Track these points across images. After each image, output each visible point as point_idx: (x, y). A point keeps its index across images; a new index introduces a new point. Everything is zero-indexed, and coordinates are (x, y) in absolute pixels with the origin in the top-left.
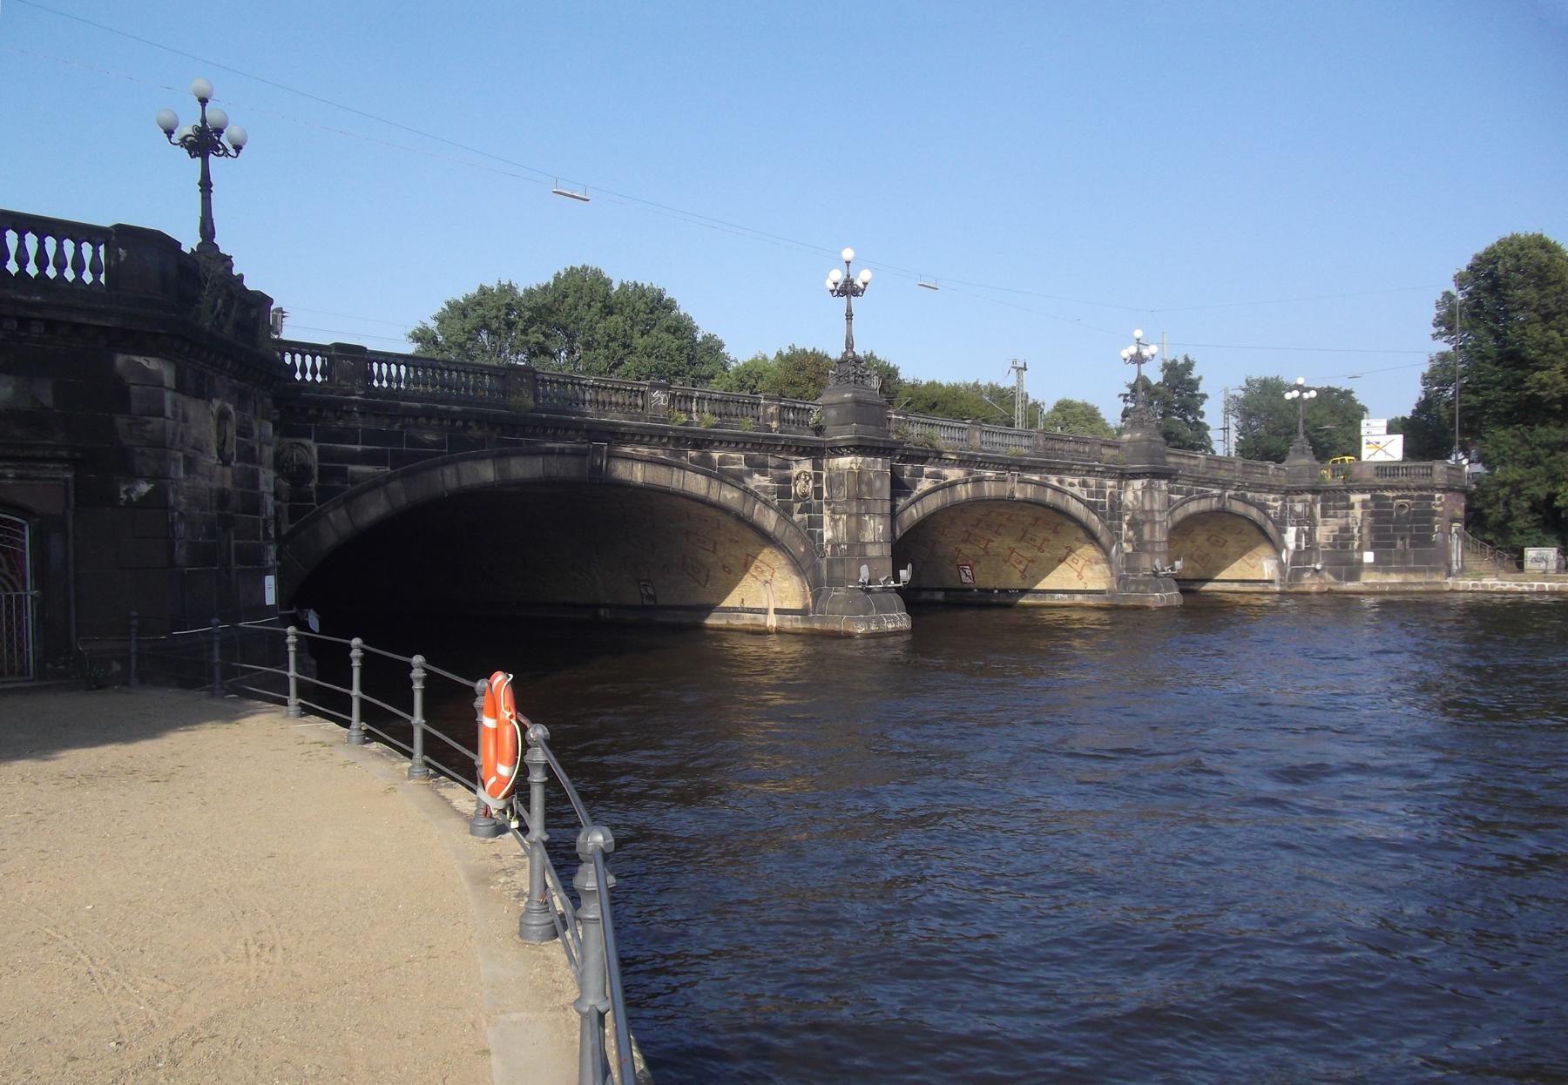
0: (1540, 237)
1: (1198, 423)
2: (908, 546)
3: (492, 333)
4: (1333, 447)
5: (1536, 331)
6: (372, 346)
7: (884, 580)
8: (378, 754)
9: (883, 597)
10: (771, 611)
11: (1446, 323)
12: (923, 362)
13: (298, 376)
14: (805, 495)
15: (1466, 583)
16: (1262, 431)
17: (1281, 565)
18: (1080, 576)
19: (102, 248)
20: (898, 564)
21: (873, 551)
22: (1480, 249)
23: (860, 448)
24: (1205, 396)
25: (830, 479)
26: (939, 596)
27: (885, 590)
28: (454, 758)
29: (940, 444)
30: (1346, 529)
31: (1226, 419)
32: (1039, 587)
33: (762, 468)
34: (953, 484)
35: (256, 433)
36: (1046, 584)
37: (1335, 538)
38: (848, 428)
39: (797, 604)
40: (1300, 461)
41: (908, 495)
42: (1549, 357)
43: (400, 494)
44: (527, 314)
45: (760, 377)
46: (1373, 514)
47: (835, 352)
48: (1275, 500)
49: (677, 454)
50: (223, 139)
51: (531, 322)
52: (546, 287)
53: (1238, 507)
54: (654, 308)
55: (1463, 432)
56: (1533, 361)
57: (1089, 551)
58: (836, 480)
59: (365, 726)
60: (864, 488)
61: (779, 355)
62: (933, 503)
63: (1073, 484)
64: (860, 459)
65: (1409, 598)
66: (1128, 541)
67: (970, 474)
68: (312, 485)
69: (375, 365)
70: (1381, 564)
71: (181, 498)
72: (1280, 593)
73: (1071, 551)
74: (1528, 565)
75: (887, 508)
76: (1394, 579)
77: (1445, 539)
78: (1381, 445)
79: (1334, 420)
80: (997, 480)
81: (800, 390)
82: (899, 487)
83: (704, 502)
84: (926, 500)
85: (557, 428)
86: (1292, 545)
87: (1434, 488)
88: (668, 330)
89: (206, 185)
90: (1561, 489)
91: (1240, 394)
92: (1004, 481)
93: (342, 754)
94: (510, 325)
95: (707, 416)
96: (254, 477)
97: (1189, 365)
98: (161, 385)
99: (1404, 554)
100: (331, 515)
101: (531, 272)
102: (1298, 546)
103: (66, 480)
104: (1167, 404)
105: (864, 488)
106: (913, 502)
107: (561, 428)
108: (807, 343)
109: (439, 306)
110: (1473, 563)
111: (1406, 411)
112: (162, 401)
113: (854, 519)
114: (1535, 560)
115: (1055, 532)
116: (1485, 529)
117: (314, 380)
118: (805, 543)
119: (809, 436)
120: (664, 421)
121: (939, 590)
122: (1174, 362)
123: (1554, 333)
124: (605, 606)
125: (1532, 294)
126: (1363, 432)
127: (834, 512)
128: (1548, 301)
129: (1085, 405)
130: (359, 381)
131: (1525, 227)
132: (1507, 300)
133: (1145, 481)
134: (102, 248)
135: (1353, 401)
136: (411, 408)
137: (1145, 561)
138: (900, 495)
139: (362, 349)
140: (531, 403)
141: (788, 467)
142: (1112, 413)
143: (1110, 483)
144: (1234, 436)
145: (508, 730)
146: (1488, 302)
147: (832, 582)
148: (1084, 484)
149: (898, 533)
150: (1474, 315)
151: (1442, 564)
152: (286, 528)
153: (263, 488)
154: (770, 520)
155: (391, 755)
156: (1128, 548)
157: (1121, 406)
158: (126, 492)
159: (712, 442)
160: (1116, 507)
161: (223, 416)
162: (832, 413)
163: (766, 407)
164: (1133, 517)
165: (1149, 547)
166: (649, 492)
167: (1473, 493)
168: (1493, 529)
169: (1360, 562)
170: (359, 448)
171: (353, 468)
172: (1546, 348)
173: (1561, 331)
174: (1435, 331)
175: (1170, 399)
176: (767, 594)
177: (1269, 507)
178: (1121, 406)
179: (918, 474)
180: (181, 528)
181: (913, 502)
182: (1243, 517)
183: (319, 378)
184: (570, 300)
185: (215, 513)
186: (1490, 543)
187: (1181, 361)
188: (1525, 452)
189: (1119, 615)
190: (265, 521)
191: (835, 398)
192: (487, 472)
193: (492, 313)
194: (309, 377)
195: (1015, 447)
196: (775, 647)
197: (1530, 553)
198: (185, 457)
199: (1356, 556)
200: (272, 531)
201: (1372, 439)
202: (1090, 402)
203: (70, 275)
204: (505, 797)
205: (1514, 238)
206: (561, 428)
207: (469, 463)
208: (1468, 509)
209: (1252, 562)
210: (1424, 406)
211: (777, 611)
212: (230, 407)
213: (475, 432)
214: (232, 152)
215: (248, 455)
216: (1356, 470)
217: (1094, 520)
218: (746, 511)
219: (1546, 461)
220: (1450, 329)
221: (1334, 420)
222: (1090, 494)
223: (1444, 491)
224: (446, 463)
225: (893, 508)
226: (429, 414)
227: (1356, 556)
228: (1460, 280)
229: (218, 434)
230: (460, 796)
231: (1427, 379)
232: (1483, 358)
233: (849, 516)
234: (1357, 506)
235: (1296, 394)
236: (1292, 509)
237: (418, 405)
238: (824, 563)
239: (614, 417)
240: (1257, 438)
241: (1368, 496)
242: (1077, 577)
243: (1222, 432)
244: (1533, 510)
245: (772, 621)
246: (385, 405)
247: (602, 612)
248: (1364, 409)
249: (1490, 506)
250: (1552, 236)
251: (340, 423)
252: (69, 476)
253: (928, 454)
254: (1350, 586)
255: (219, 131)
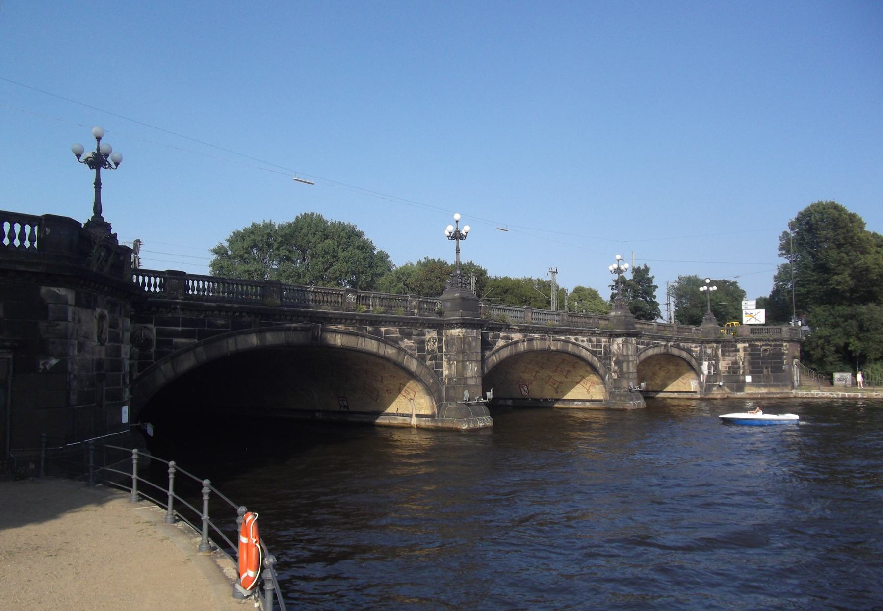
0: (834, 203)
1: (652, 301)
2: (491, 378)
3: (259, 249)
4: (727, 314)
5: (833, 253)
6: (189, 271)
7: (478, 398)
8: (182, 531)
9: (477, 407)
10: (414, 416)
11: (786, 247)
12: (500, 266)
13: (146, 289)
14: (433, 350)
15: (803, 393)
16: (688, 305)
17: (700, 383)
18: (588, 392)
19: (36, 228)
20: (485, 390)
21: (472, 382)
22: (802, 209)
23: (463, 324)
24: (656, 287)
25: (447, 341)
26: (510, 402)
27: (478, 404)
28: (225, 540)
29: (509, 320)
30: (735, 363)
31: (668, 299)
32: (565, 397)
33: (409, 336)
34: (516, 342)
35: (121, 325)
36: (569, 396)
37: (730, 368)
38: (457, 313)
39: (428, 412)
40: (709, 325)
41: (491, 349)
42: (841, 267)
43: (203, 354)
44: (280, 239)
45: (409, 274)
46: (750, 355)
47: (451, 261)
48: (696, 347)
49: (361, 329)
50: (109, 159)
51: (281, 244)
52: (290, 224)
53: (675, 351)
54: (349, 237)
55: (797, 307)
56: (834, 269)
57: (594, 378)
58: (451, 341)
59: (175, 513)
60: (466, 346)
61: (419, 263)
62: (505, 353)
63: (583, 340)
64: (464, 330)
65: (773, 402)
66: (615, 372)
67: (526, 336)
68: (152, 350)
69: (190, 282)
70: (755, 383)
71: (75, 367)
72: (701, 399)
73: (583, 377)
74: (836, 382)
75: (479, 357)
76: (764, 390)
77: (790, 369)
78: (753, 315)
79: (727, 300)
80: (541, 339)
81: (431, 283)
82: (486, 345)
83: (376, 355)
84: (501, 352)
85: (293, 316)
86: (706, 372)
87: (782, 340)
88: (358, 247)
89: (98, 185)
90: (851, 340)
91: (676, 285)
92: (545, 340)
93: (161, 532)
94: (270, 245)
95: (378, 307)
96: (118, 350)
97: (647, 270)
98: (66, 303)
99: (768, 377)
100: (162, 367)
101: (282, 215)
102: (709, 373)
103: (9, 359)
104: (635, 291)
105: (466, 346)
106: (494, 353)
107: (296, 316)
108: (435, 256)
109: (228, 234)
110: (807, 381)
111: (767, 293)
112: (66, 313)
113: (460, 364)
114: (840, 380)
115: (574, 367)
116: (812, 362)
117: (155, 291)
118: (433, 377)
119: (435, 317)
120: (353, 311)
121: (510, 399)
122: (639, 268)
123: (843, 255)
124: (319, 411)
125: (831, 234)
126: (743, 308)
127: (449, 360)
128: (840, 237)
129: (590, 290)
130: (181, 291)
131: (826, 197)
132: (821, 236)
133: (624, 339)
134: (36, 228)
135: (737, 287)
136: (209, 306)
137: (624, 383)
138: (487, 349)
139: (182, 274)
140: (278, 302)
141: (424, 335)
142: (605, 295)
143: (604, 340)
144: (673, 308)
145: (254, 550)
146: (808, 237)
147: (449, 399)
148: (590, 341)
149: (486, 371)
150: (800, 244)
151: (789, 383)
152: (136, 375)
153: (123, 356)
154: (413, 365)
155: (190, 531)
156: (615, 376)
157: (610, 292)
158: (43, 365)
159: (381, 322)
160: (608, 353)
161: (102, 317)
162: (448, 304)
163: (411, 301)
164: (617, 359)
165: (626, 375)
166: (345, 351)
167: (804, 342)
168: (817, 363)
169: (744, 381)
170: (180, 329)
171: (176, 340)
172: (839, 262)
173: (847, 253)
174: (780, 252)
175: (637, 289)
176: (411, 406)
177: (693, 351)
178: (610, 292)
179: (497, 337)
180: (74, 384)
181: (494, 353)
182: (679, 357)
183: (158, 290)
184: (304, 231)
185: (95, 373)
186: (814, 370)
187: (642, 267)
188: (831, 320)
189: (613, 415)
190: (124, 375)
191: (449, 296)
192: (253, 340)
193: (257, 241)
194: (152, 289)
195: (551, 320)
196: (416, 438)
197: (837, 375)
198: (79, 343)
199: (741, 378)
200: (127, 381)
201: (748, 312)
202: (593, 288)
203: (17, 243)
204: (251, 589)
205: (820, 203)
206: (296, 316)
207: (242, 336)
208: (801, 351)
209: (684, 381)
210: (776, 292)
211: (417, 416)
212: (106, 312)
213: (247, 319)
214: (114, 166)
215: (116, 338)
216: (740, 330)
217: (596, 361)
218: (400, 360)
219: (843, 325)
220: (788, 252)
221: (727, 300)
222: (593, 346)
223: (788, 341)
224: (229, 336)
225: (483, 356)
226: (220, 309)
227: (741, 378)
228: (792, 226)
229: (99, 328)
230: (228, 567)
231: (777, 278)
232: (806, 267)
233: (458, 362)
234: (741, 350)
235: (705, 288)
236: (705, 352)
237: (214, 304)
238: (444, 389)
239: (325, 309)
240: (685, 309)
241: (747, 345)
242: (586, 392)
243: (666, 308)
244: (837, 351)
245: (414, 421)
246: (196, 304)
247: (317, 414)
248: (744, 292)
249: (813, 349)
250: (840, 202)
251: (169, 315)
252: (10, 356)
253: (503, 326)
254: (739, 395)
255: (107, 156)
